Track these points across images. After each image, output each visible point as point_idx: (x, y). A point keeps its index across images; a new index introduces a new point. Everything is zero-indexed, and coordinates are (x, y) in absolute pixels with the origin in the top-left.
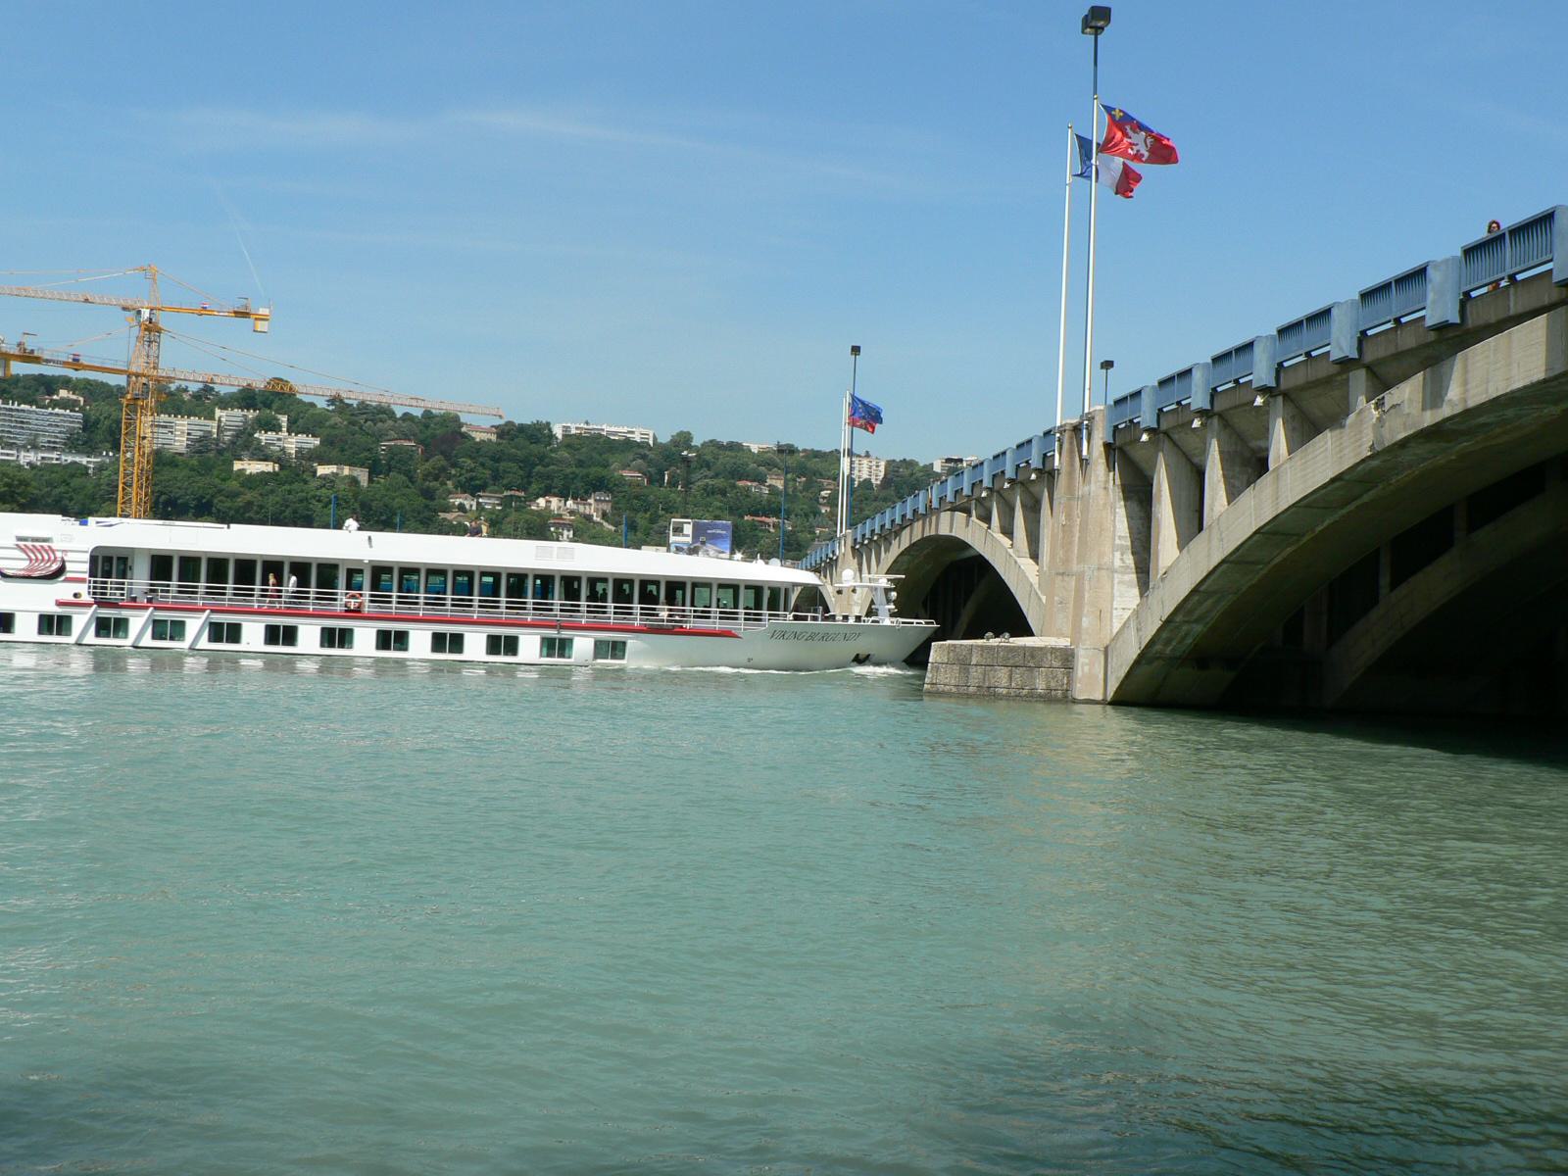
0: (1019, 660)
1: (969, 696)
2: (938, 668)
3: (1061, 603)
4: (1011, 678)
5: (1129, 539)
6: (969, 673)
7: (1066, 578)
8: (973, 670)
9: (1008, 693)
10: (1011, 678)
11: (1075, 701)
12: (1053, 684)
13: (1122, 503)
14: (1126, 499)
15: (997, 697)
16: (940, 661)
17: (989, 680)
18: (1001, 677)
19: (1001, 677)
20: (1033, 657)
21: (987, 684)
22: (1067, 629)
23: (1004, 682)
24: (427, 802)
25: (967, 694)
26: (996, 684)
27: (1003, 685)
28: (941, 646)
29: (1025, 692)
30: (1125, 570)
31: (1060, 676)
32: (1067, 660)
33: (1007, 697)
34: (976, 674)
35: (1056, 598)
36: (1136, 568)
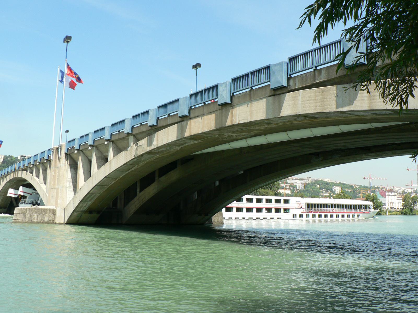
0: (40, 212)
1: (25, 222)
2: (17, 215)
3: (52, 196)
7: (54, 189)
8: (27, 215)
11: (56, 224)
12: (50, 219)
13: (70, 169)
14: (71, 168)
15: (34, 223)
17: (32, 218)
18: (35, 217)
19: (35, 217)
20: (44, 211)
21: (31, 219)
23: (36, 218)
29: (42, 221)
30: (70, 187)
31: (52, 216)
32: (54, 212)
33: (37, 223)
34: (28, 217)
35: (51, 195)
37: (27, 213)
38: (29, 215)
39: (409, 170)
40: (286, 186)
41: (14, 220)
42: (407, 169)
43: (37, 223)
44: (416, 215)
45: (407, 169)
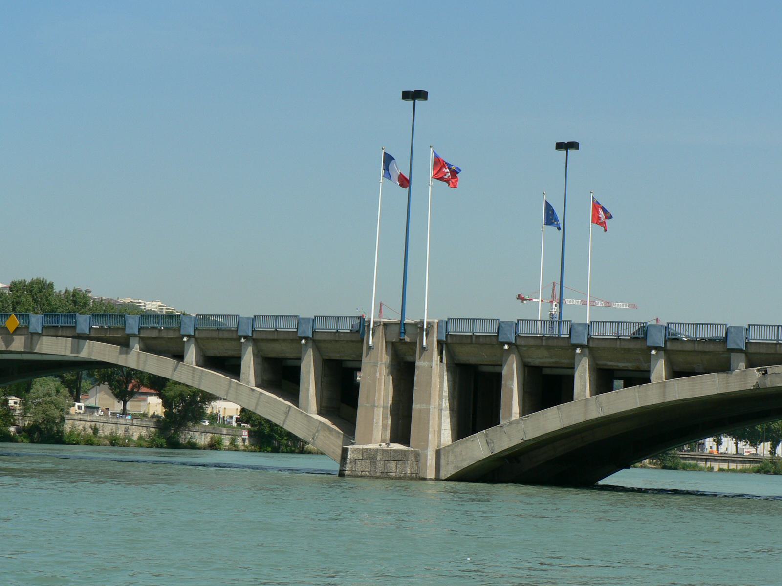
0: (399, 457)
1: (377, 477)
4: (397, 467)
5: (447, 392)
6: (376, 464)
8: (378, 463)
9: (396, 475)
10: (396, 467)
15: (390, 478)
16: (357, 458)
20: (405, 455)
22: (232, 384)
24: (60, 472)
25: (376, 477)
26: (391, 471)
27: (393, 471)
28: (90, 342)
32: (417, 457)
33: (396, 478)
34: (380, 465)
35: (375, 420)
36: (450, 408)
37: (379, 459)
38: (382, 462)
39: (523, 300)
40: (71, 304)
41: (350, 472)
42: (519, 297)
43: (396, 478)
44: (488, 445)
45: (519, 297)
